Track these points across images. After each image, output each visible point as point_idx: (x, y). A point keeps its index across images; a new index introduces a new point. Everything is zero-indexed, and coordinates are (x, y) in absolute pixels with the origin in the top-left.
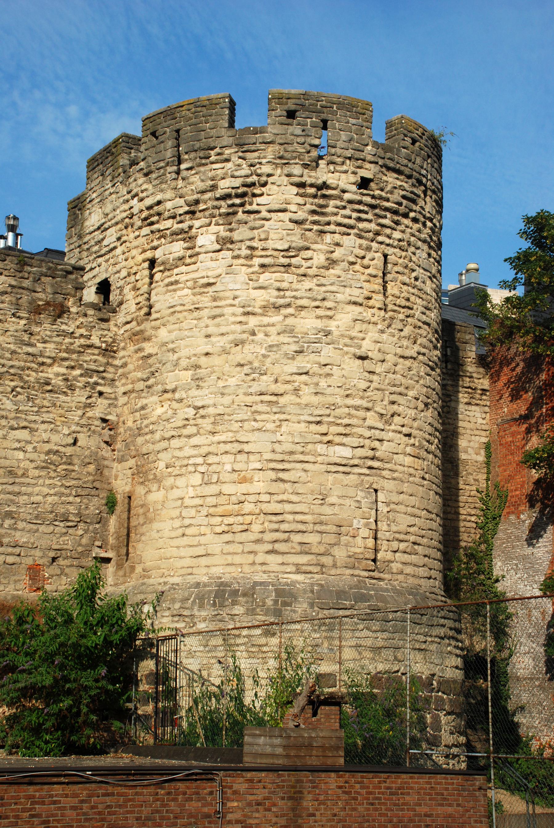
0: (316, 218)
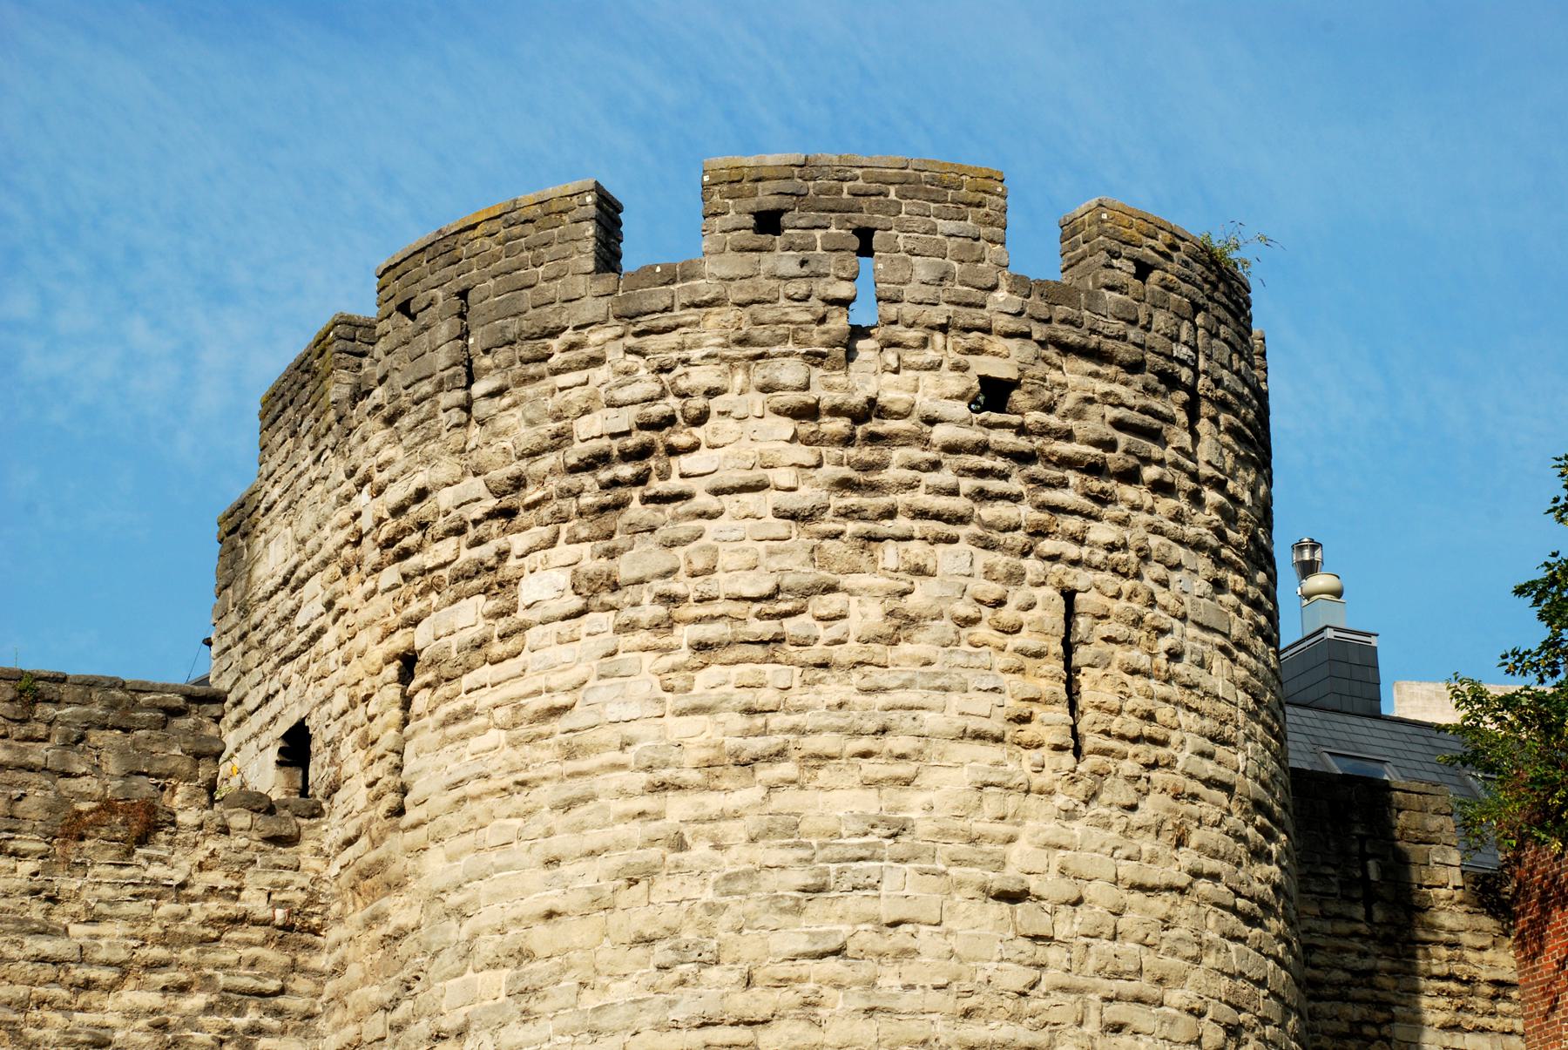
0: (853, 500)
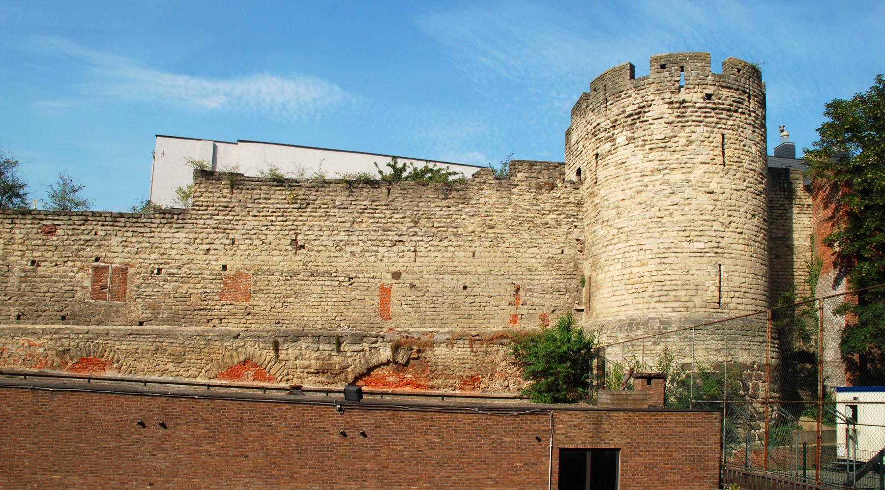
0: (680, 119)
